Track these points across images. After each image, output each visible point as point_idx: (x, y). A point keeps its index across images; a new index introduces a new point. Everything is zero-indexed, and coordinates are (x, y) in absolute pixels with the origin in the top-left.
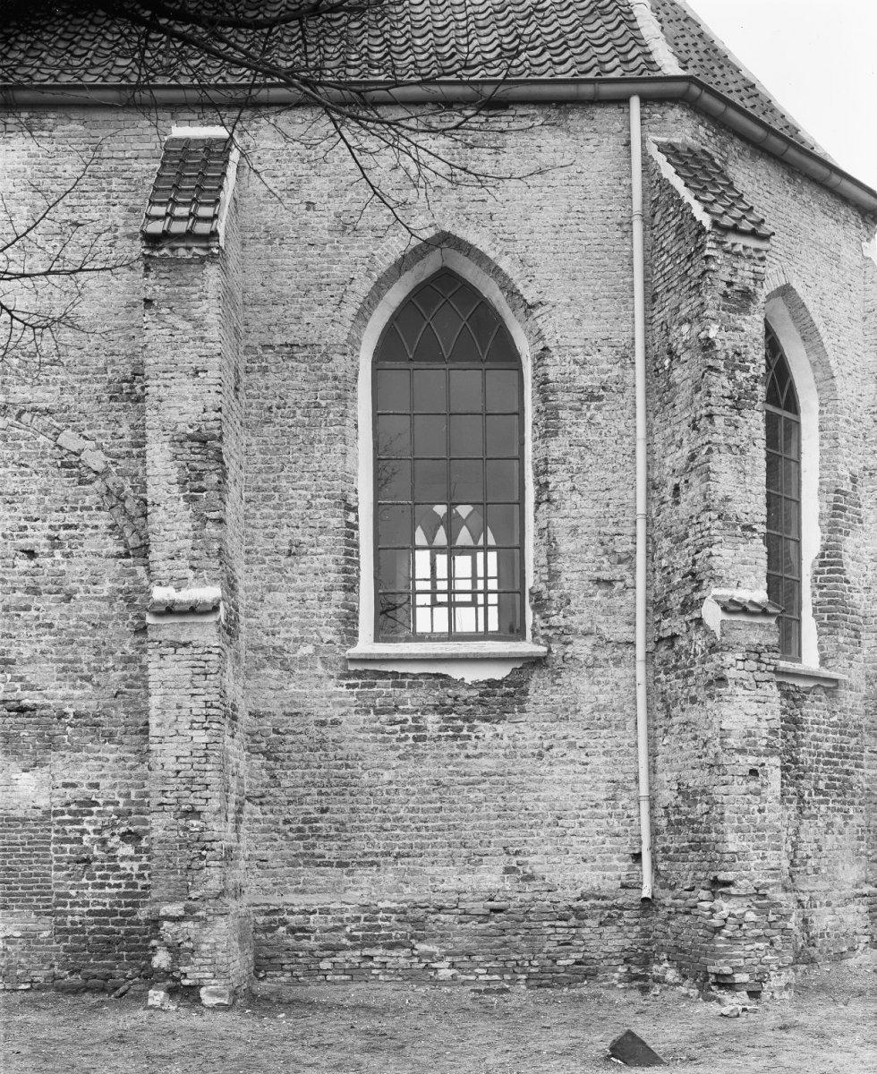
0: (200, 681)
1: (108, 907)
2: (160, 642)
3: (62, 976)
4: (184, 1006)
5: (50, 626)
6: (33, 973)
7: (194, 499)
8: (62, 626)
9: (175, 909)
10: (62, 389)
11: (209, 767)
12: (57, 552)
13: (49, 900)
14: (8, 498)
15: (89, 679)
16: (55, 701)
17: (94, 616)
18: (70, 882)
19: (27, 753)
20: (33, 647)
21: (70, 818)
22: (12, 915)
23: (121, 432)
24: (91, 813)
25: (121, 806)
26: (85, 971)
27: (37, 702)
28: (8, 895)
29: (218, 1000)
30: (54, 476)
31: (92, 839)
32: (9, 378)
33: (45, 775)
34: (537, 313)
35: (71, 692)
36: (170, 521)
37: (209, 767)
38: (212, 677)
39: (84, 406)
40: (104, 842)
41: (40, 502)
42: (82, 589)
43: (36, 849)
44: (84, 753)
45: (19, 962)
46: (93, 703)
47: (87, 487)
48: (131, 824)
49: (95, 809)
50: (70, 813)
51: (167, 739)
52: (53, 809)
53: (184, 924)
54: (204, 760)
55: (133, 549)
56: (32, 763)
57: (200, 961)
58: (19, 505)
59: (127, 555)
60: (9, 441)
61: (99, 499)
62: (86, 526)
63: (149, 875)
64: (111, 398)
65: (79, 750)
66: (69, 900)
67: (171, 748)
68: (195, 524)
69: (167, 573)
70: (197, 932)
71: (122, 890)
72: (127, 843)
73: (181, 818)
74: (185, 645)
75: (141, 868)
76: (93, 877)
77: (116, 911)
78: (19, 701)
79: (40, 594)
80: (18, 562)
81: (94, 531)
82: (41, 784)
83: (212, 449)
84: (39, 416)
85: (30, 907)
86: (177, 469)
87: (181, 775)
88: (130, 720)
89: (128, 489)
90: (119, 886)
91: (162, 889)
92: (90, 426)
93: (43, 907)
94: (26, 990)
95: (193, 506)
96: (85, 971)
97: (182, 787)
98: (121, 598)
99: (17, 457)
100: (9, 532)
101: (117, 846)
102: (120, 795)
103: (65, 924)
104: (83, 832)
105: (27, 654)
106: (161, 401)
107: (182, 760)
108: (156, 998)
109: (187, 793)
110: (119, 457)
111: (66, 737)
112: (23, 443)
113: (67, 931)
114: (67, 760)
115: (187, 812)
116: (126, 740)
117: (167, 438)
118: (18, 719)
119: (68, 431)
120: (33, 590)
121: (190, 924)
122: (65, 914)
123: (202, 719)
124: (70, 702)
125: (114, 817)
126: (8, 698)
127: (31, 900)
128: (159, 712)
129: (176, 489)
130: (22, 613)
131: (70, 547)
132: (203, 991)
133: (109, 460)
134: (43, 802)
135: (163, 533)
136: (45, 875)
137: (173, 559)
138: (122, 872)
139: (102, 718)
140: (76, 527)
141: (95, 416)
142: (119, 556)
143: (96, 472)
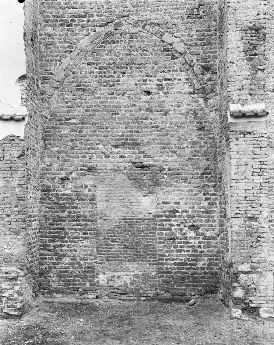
0: (257, 151)
1: (183, 261)
2: (236, 132)
3: (161, 294)
4: (252, 318)
5: (157, 127)
6: (148, 292)
7: (252, 59)
8: (163, 127)
9: (246, 267)
10: (165, 13)
11: (262, 195)
12: (160, 92)
13: (155, 258)
14: (138, 66)
15: (175, 152)
16: (159, 163)
17: (178, 122)
18: (165, 249)
19: (145, 187)
20: (149, 137)
21: (165, 218)
22: (138, 264)
23: (192, 33)
24: (175, 216)
25: (190, 213)
26: (172, 291)
27: (150, 163)
28: (136, 255)
29: (269, 315)
30: (160, 55)
31: (176, 229)
32: (139, 8)
34: (26, 98)
35: (167, 158)
36: (239, 71)
37: (262, 195)
38: (264, 149)
39: (175, 21)
40: (181, 230)
41: (153, 68)
42: (172, 109)
43: (149, 233)
44: (172, 188)
45: (141, 287)
46: (177, 164)
47: (175, 60)
48: (194, 222)
49: (177, 214)
50: (165, 216)
51: (240, 181)
52: (157, 214)
53: (251, 275)
54: (259, 191)
55: (197, 90)
56: (148, 192)
57: (259, 294)
58: (143, 69)
59: (194, 93)
60: (139, 39)
61: (181, 66)
62: (175, 79)
63: (203, 246)
64: (188, 17)
65: (170, 186)
66: (165, 258)
67: (242, 185)
68: (252, 72)
69: (237, 97)
70: (258, 280)
71: (190, 253)
72: (191, 231)
74: (249, 133)
75: (199, 243)
76: (176, 247)
77: (187, 263)
79: (153, 112)
80: (142, 96)
81: (179, 82)
82: (152, 202)
83: (261, 34)
84: (153, 27)
85: (146, 261)
86: (243, 44)
87: (247, 199)
88: (195, 172)
89: (195, 61)
90: (189, 251)
91: (238, 257)
92: (178, 31)
93: (153, 261)
94: (144, 300)
95: (252, 63)
96: (172, 291)
98: (191, 114)
99: (142, 47)
100: (138, 82)
101: (187, 232)
102: (189, 208)
103: (163, 269)
104: (172, 225)
105: (146, 140)
106: (235, 10)
107: (248, 191)
108: (237, 313)
109: (251, 208)
110: (191, 46)
111: (164, 180)
112: (145, 40)
113: (164, 272)
114: (164, 191)
115: (250, 218)
116: (193, 181)
117: (239, 29)
118: (141, 171)
119: (167, 34)
120: (150, 110)
121: (254, 275)
122: (163, 264)
123: (258, 170)
124: (166, 163)
125: (186, 218)
126: (137, 161)
127: (147, 257)
128: (236, 167)
129: (242, 54)
130: (144, 121)
131: (167, 89)
132: (261, 310)
133: (186, 47)
134: (153, 211)
135: (235, 77)
136: (154, 245)
137: (240, 90)
138: (190, 245)
139: (181, 171)
140: (170, 80)
141: (180, 26)
142: (191, 93)
143: (180, 53)
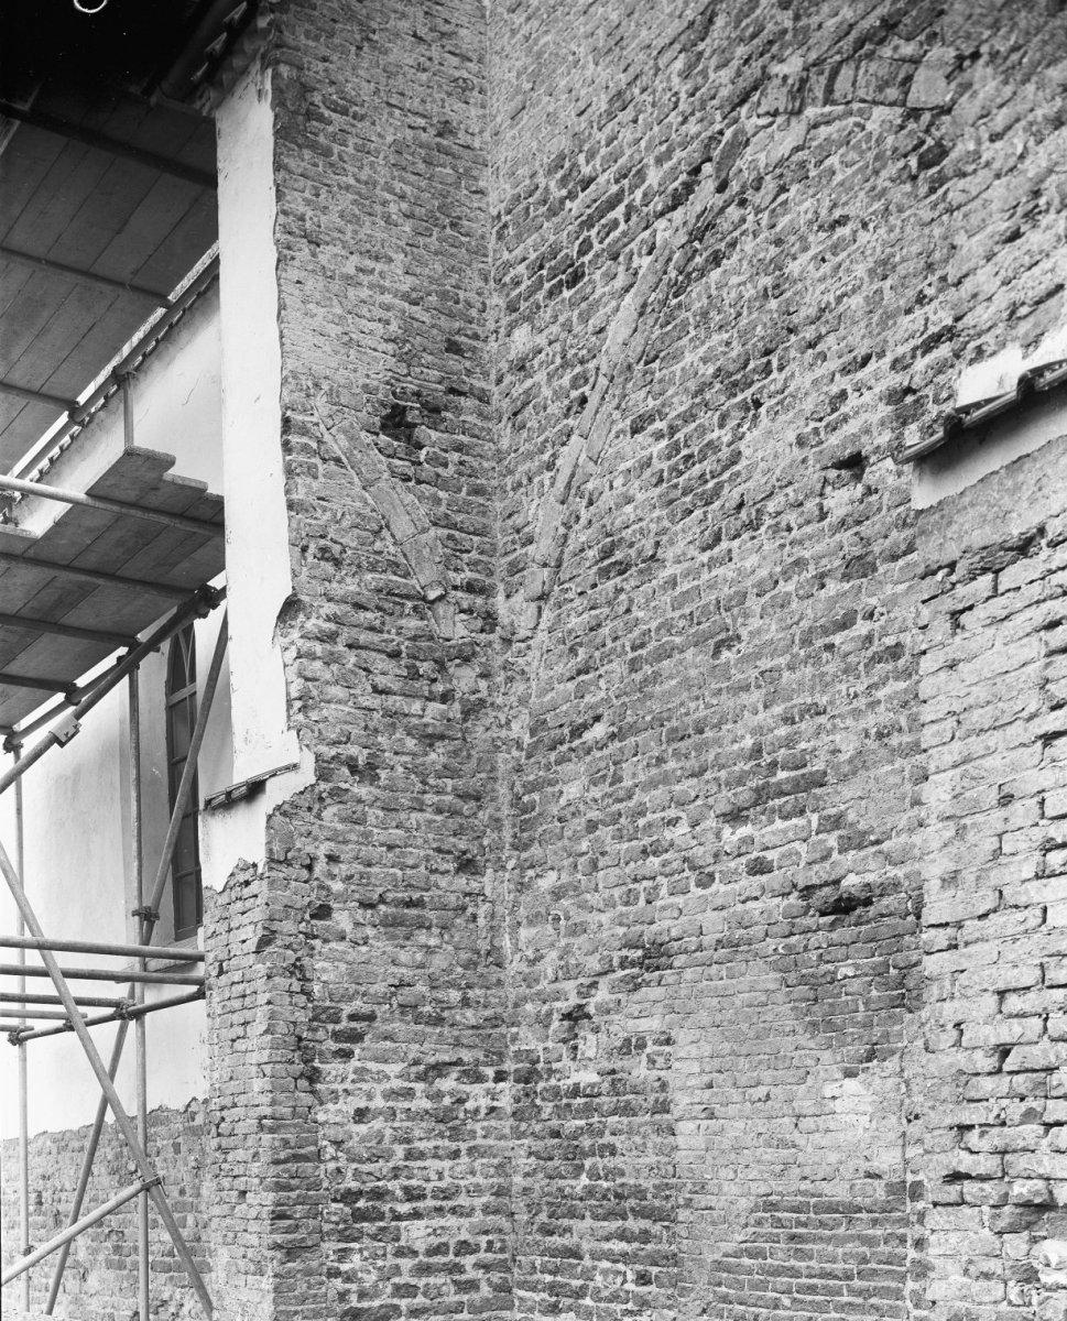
2: (952, 566)
20: (862, 724)
27: (870, 878)
33: (891, 1082)
56: (863, 1050)
73: (1013, 1229)
74: (1024, 548)
78: (837, 882)
82: (881, 1112)
87: (1011, 1063)
97: (1016, 1110)
126: (816, 881)
